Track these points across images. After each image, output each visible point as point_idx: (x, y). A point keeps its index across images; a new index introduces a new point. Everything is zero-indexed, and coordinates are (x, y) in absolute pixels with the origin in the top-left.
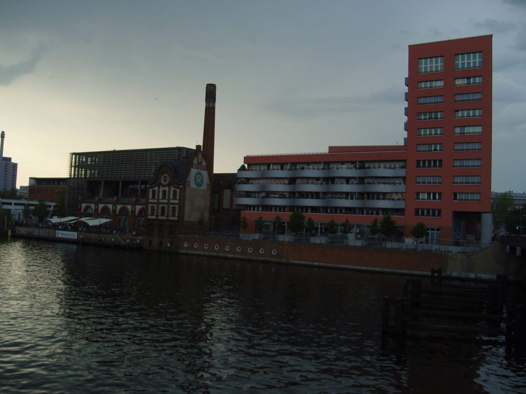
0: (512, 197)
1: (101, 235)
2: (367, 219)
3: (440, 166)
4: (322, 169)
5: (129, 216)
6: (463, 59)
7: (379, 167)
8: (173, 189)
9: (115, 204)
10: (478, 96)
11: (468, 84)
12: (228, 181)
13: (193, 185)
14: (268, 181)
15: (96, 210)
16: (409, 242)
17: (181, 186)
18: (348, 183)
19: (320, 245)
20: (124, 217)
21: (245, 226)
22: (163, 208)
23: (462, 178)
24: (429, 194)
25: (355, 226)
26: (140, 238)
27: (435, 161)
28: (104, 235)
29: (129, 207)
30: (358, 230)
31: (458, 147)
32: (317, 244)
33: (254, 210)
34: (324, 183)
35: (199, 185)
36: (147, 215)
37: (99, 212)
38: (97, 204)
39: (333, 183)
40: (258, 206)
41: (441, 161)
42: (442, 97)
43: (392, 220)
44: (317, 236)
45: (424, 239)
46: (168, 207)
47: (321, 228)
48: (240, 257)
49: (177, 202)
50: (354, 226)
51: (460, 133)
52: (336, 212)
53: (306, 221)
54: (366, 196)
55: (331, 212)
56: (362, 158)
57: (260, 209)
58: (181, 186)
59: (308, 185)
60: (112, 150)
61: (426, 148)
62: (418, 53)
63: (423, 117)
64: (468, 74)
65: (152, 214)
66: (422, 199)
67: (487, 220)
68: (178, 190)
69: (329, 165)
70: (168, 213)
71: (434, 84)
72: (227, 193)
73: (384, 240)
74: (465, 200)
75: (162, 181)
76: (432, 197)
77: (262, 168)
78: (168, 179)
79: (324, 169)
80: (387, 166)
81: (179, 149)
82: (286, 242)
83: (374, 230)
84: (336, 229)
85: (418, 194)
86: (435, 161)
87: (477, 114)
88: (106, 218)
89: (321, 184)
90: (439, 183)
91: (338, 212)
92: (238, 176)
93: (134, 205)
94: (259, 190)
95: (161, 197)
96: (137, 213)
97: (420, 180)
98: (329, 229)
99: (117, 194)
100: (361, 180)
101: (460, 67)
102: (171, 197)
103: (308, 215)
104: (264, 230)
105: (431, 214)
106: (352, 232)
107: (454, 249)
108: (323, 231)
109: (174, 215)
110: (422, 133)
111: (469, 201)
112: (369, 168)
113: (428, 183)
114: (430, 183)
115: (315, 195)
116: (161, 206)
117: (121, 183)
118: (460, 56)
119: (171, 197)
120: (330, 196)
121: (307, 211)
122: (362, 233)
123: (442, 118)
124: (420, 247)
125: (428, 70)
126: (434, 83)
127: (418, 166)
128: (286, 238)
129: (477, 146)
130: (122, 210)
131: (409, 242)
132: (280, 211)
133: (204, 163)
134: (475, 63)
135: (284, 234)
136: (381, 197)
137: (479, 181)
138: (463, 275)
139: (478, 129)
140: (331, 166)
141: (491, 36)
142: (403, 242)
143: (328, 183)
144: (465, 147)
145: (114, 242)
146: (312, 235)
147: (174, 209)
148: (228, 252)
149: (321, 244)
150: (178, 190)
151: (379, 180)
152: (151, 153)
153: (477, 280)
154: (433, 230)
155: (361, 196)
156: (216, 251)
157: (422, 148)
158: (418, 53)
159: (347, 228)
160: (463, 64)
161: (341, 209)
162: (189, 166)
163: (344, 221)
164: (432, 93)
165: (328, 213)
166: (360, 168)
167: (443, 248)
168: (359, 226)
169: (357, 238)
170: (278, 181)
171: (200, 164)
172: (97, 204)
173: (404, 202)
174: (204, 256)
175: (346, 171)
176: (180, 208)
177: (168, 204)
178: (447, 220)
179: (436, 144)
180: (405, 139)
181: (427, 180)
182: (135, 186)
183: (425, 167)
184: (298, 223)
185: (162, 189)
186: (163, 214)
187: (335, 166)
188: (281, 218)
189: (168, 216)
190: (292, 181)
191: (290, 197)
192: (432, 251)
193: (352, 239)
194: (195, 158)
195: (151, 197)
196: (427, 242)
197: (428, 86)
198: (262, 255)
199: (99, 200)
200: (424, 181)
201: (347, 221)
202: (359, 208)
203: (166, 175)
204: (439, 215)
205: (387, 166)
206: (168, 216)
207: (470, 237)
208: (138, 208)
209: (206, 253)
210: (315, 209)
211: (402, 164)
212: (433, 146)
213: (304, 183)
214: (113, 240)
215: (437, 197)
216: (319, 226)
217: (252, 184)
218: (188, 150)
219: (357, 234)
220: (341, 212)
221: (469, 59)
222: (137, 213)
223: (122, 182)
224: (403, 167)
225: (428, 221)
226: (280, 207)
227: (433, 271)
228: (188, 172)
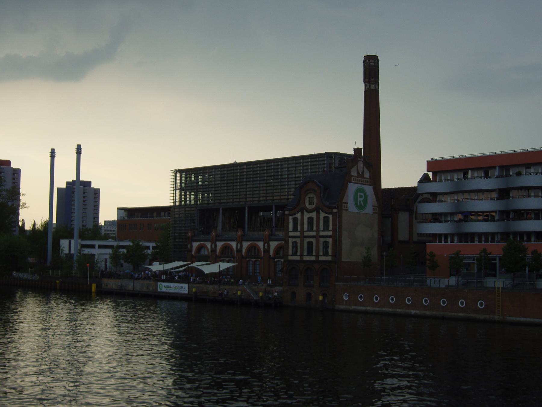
1: (222, 287)
4: (497, 177)
5: (261, 258)
8: (322, 215)
9: (240, 241)
12: (404, 198)
13: (352, 208)
14: (466, 196)
15: (214, 251)
17: (335, 211)
20: (254, 260)
22: (310, 244)
28: (227, 287)
29: (261, 244)
33: (446, 241)
35: (361, 207)
37: (218, 253)
40: (452, 235)
48: (428, 313)
49: (330, 233)
57: (456, 239)
58: (335, 211)
60: (232, 162)
65: (295, 254)
68: (331, 216)
72: (403, 217)
78: (315, 200)
81: (329, 156)
82: (499, 288)
92: (419, 191)
99: (242, 227)
102: (321, 228)
104: (464, 271)
109: (326, 254)
116: (306, 240)
119: (321, 228)
121: (529, 240)
128: (498, 282)
130: (249, 249)
133: (367, 175)
135: (494, 276)
145: (240, 296)
150: (331, 216)
152: (288, 164)
156: (391, 306)
170: (481, 195)
176: (334, 242)
185: (307, 216)
186: (310, 253)
189: (317, 256)
190: (504, 194)
194: (353, 167)
195: (291, 228)
199: (217, 236)
203: (311, 195)
206: (317, 256)
209: (377, 309)
213: (523, 196)
214: (239, 293)
217: (440, 201)
218: (342, 156)
223: (249, 208)
226: (486, 235)
228: (344, 189)
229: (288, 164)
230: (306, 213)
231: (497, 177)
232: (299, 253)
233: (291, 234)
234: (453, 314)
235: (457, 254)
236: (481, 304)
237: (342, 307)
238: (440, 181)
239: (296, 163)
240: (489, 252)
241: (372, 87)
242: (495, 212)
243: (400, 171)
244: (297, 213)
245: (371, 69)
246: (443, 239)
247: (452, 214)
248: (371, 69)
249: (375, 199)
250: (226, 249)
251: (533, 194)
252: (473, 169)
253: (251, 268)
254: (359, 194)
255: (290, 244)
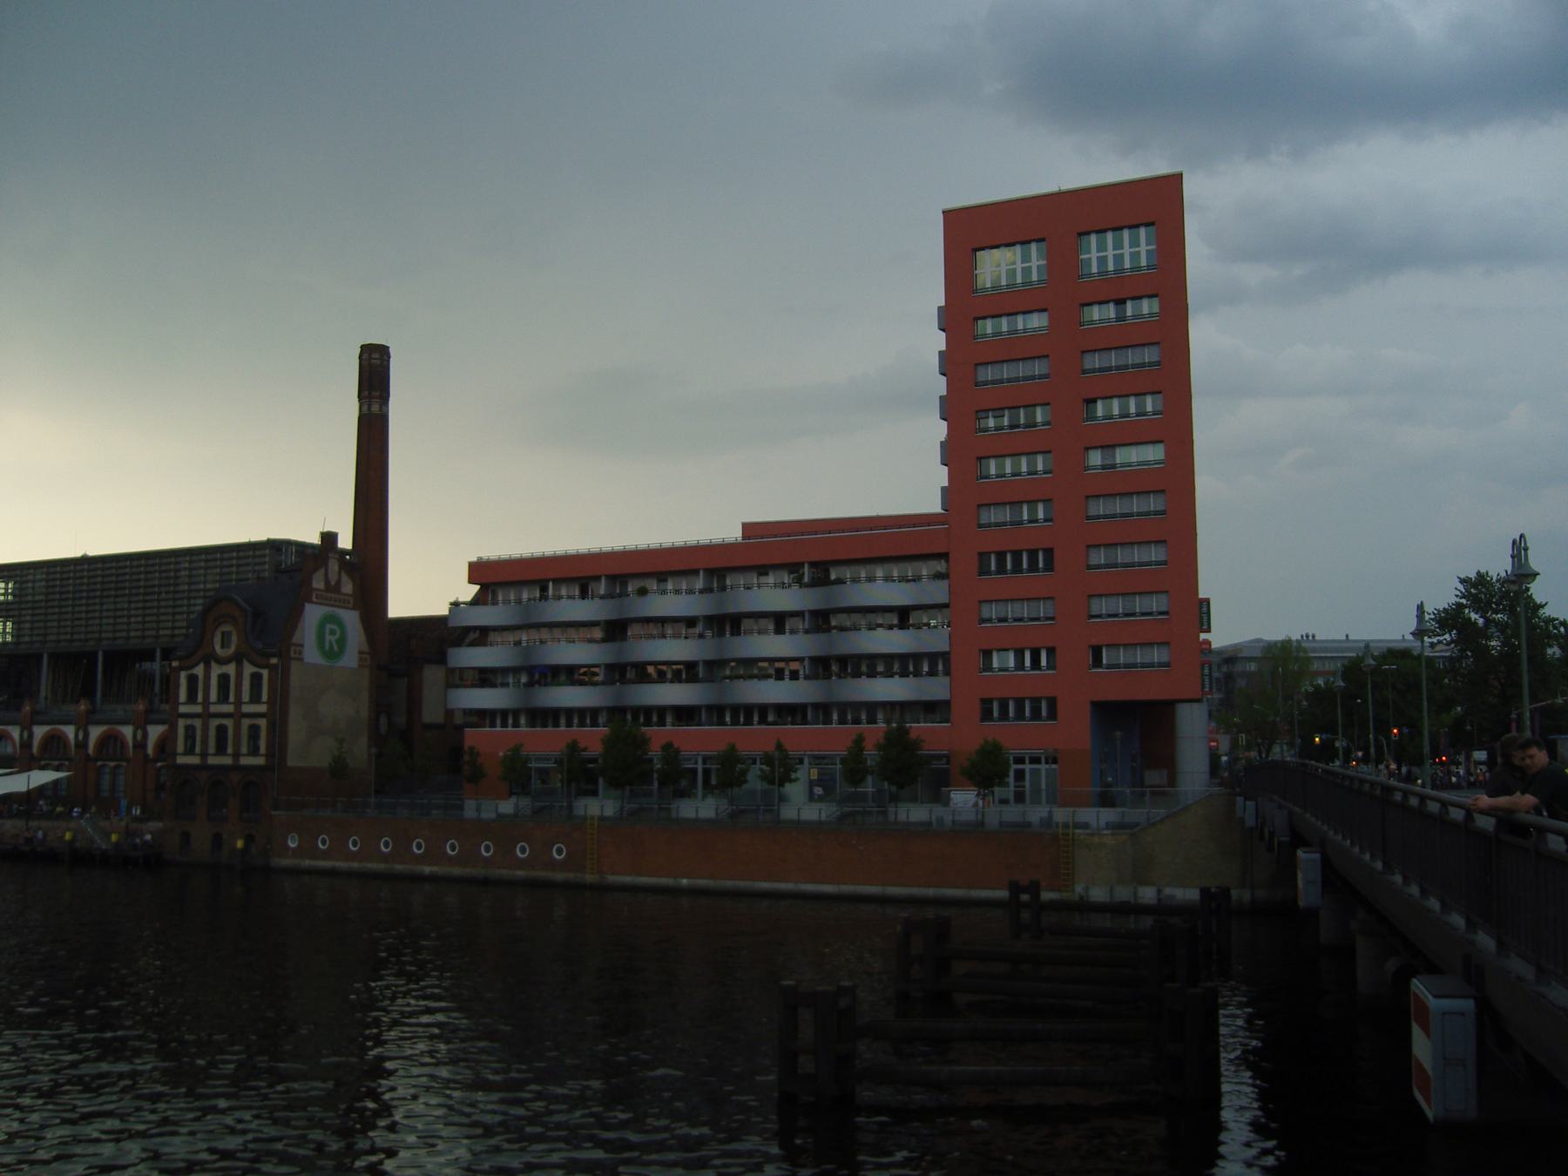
0: (1305, 651)
1: (33, 824)
2: (834, 738)
3: (1049, 566)
4: (701, 592)
5: (128, 761)
6: (1102, 247)
7: (871, 579)
8: (249, 669)
9: (83, 724)
10: (1149, 355)
11: (1118, 319)
12: (431, 637)
13: (312, 655)
14: (545, 634)
15: (26, 745)
16: (963, 799)
17: (274, 661)
18: (780, 630)
19: (697, 824)
20: (112, 764)
21: (477, 776)
22: (221, 730)
23: (1113, 600)
24: (1019, 654)
25: (806, 761)
26: (155, 825)
27: (1033, 554)
28: (44, 824)
29: (127, 731)
30: (814, 774)
31: (1099, 508)
32: (807, 823)
33: (504, 725)
34: (709, 633)
35: (331, 654)
36: (175, 754)
37: (35, 750)
38: (27, 727)
39: (736, 631)
40: (516, 713)
41: (1049, 553)
42: (1045, 362)
43: (913, 736)
44: (695, 796)
45: (1009, 791)
46: (238, 727)
47: (707, 772)
48: (457, 871)
49: (262, 708)
50: (801, 762)
51: (1103, 467)
52: (748, 722)
53: (655, 751)
54: (834, 668)
55: (735, 722)
56: (811, 555)
57: (523, 721)
58: (274, 661)
59: (660, 643)
60: (79, 554)
61: (1005, 515)
62: (969, 231)
63: (991, 423)
64: (1119, 290)
65: (190, 751)
66: (1001, 670)
67: (1193, 724)
68: (265, 673)
69: (722, 578)
70: (237, 744)
71: (1020, 322)
72: (432, 676)
73: (895, 799)
74: (1126, 666)
75: (218, 648)
76: (1028, 663)
77: (525, 596)
78: (234, 638)
79: (707, 590)
80: (895, 574)
81: (276, 547)
82: (592, 818)
83: (855, 770)
84: (744, 773)
85: (987, 654)
86: (1033, 554)
87: (1149, 408)
88: (57, 769)
89: (701, 636)
90: (1048, 619)
91: (756, 718)
92: (451, 624)
93: (141, 724)
94: (506, 664)
95: (213, 696)
96: (150, 750)
97: (991, 611)
98: (726, 773)
99: (88, 693)
100: (820, 620)
101: (1094, 270)
102: (246, 697)
103: (669, 731)
104: (536, 784)
105: (1027, 714)
106: (796, 780)
107: (1088, 815)
108: (714, 781)
109: (254, 751)
110: (993, 471)
111: (1139, 670)
112: (840, 581)
113: (1016, 620)
114: (1021, 620)
115: (687, 672)
116: (214, 723)
117: (100, 658)
118: (1093, 238)
119: (246, 697)
120: (728, 672)
121: (662, 723)
122: (825, 781)
123: (1048, 423)
124: (995, 815)
125: (1127, 265)
126: (1020, 318)
127: (984, 570)
128: (599, 807)
129: (1154, 503)
130: (104, 741)
131: (963, 799)
132: (582, 724)
133: (348, 587)
134: (1135, 256)
135: (594, 793)
136: (880, 668)
137: (1164, 609)
138: (1123, 894)
139: (1153, 454)
140: (728, 582)
141: (1175, 181)
142: (946, 802)
143: (721, 634)
144: (1118, 506)
145: (73, 841)
146: (682, 794)
147: (254, 731)
148: (420, 860)
149: (697, 820)
150: (265, 673)
151: (871, 617)
152: (191, 562)
153: (1162, 910)
154: (1035, 760)
155: (821, 666)
156: (385, 858)
157: (992, 516)
158: (969, 231)
159: (781, 768)
160: (1102, 261)
161: (763, 709)
162: (299, 596)
163: (770, 748)
164: (1014, 350)
165: (724, 724)
166: (814, 583)
167: (1061, 815)
168: (818, 760)
169: (811, 798)
170: (572, 633)
171: (336, 589)
172: (27, 727)
173: (947, 679)
174: (350, 874)
175: (774, 595)
176: (272, 726)
177: (238, 716)
178: (1074, 731)
179: (1032, 503)
180: (943, 489)
181: (1011, 610)
182: (147, 665)
183: (1037, 570)
184: (628, 760)
185: (216, 671)
186: (221, 750)
187: (741, 580)
188: (582, 746)
189: (236, 755)
190: (615, 630)
191: (608, 682)
192: (1029, 825)
193: (800, 804)
194: (315, 570)
195: (183, 696)
196: (1020, 798)
197: (1005, 328)
198: (523, 864)
199: (35, 713)
200: (1002, 615)
201: (779, 747)
202: (816, 706)
203: (227, 628)
204: (1053, 715)
205: (895, 574)
206: (236, 755)
207: (1154, 777)
208: (155, 732)
209: (355, 865)
210: (685, 714)
211: (941, 566)
212: (1025, 508)
213: (652, 637)
214: (68, 836)
215: (1044, 662)
216: (700, 767)
217: (918, 627)
218: (302, 547)
219: (812, 784)
220: (763, 720)
221: (1118, 245)
222: (150, 750)
223: (106, 654)
224: (939, 576)
225: (1015, 736)
226: (582, 712)
227: (1015, 889)
228: (298, 612)
229: (191, 562)
230: (246, 665)
231: (602, 597)
232: (198, 750)
233: (183, 709)
234: (504, 872)
235: (516, 750)
236: (559, 851)
237: (285, 862)
238: (495, 603)
239: (207, 561)
240: (582, 746)
241: (375, 408)
242: (800, 660)
243: (424, 583)
244: (197, 664)
245: (374, 372)
246: (498, 721)
247: (516, 671)
248: (374, 372)
249: (363, 638)
250: (54, 743)
251: (669, 631)
252: (558, 581)
253: (106, 781)
254: (329, 627)
255: (181, 731)
